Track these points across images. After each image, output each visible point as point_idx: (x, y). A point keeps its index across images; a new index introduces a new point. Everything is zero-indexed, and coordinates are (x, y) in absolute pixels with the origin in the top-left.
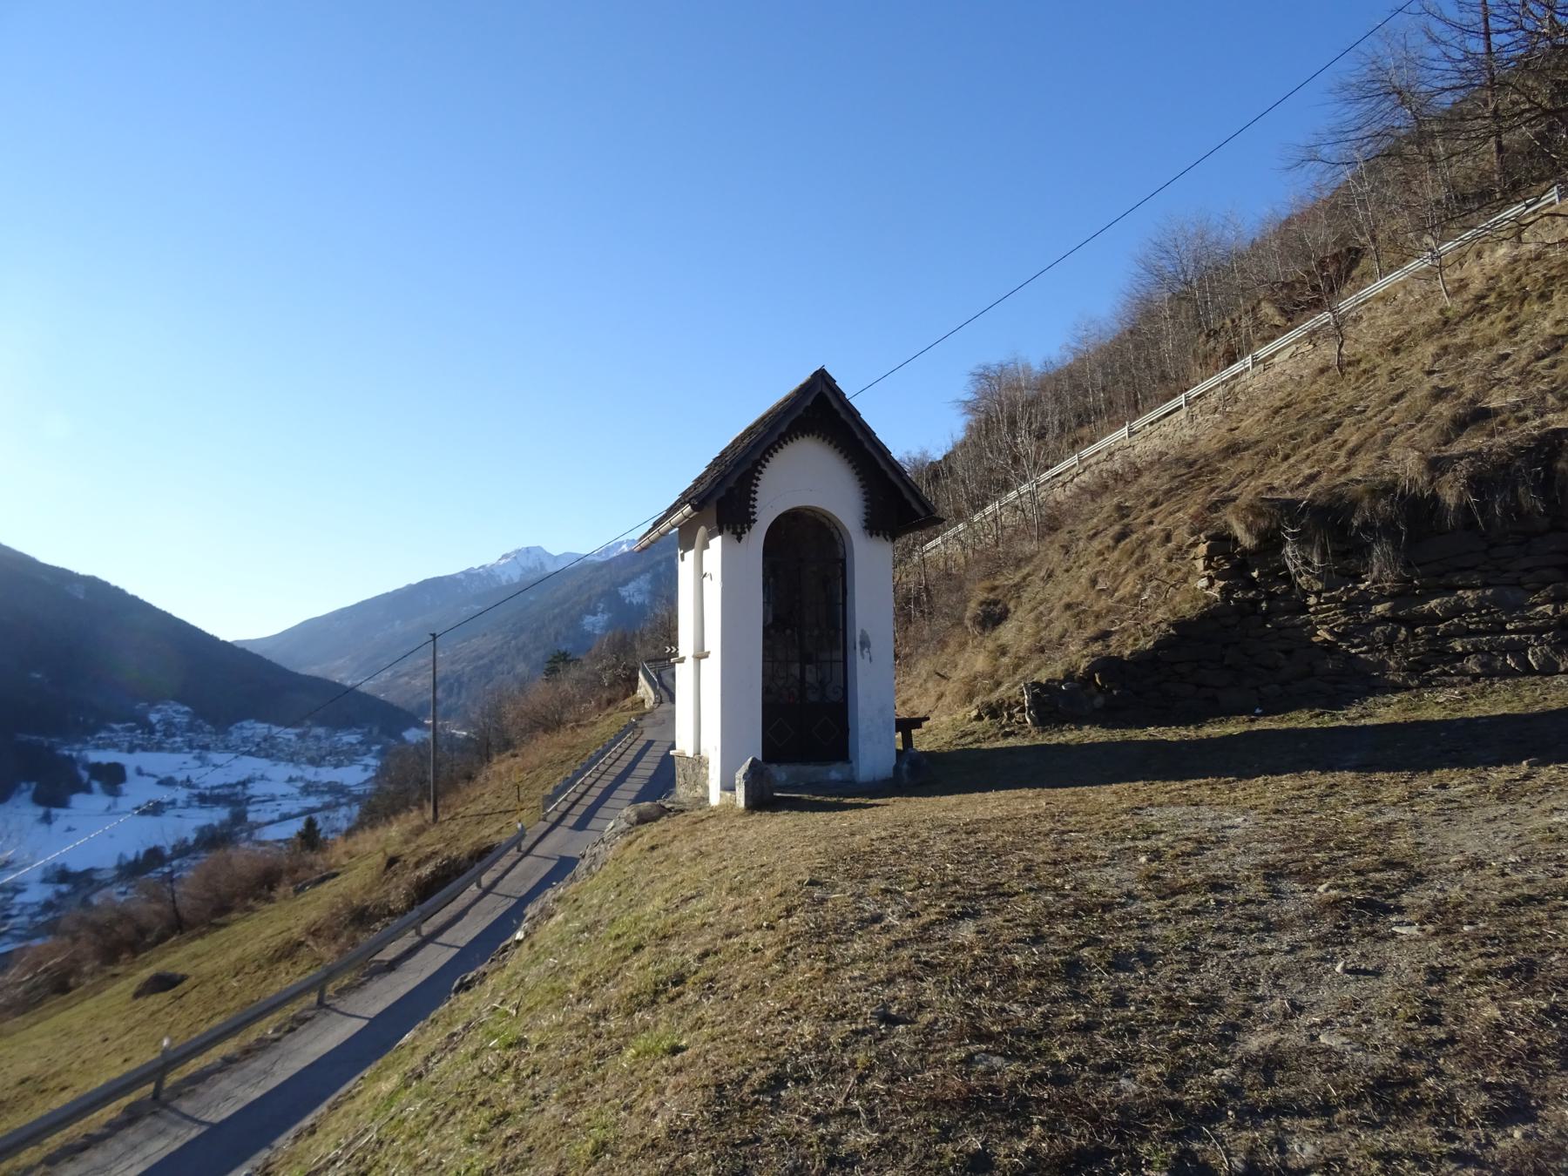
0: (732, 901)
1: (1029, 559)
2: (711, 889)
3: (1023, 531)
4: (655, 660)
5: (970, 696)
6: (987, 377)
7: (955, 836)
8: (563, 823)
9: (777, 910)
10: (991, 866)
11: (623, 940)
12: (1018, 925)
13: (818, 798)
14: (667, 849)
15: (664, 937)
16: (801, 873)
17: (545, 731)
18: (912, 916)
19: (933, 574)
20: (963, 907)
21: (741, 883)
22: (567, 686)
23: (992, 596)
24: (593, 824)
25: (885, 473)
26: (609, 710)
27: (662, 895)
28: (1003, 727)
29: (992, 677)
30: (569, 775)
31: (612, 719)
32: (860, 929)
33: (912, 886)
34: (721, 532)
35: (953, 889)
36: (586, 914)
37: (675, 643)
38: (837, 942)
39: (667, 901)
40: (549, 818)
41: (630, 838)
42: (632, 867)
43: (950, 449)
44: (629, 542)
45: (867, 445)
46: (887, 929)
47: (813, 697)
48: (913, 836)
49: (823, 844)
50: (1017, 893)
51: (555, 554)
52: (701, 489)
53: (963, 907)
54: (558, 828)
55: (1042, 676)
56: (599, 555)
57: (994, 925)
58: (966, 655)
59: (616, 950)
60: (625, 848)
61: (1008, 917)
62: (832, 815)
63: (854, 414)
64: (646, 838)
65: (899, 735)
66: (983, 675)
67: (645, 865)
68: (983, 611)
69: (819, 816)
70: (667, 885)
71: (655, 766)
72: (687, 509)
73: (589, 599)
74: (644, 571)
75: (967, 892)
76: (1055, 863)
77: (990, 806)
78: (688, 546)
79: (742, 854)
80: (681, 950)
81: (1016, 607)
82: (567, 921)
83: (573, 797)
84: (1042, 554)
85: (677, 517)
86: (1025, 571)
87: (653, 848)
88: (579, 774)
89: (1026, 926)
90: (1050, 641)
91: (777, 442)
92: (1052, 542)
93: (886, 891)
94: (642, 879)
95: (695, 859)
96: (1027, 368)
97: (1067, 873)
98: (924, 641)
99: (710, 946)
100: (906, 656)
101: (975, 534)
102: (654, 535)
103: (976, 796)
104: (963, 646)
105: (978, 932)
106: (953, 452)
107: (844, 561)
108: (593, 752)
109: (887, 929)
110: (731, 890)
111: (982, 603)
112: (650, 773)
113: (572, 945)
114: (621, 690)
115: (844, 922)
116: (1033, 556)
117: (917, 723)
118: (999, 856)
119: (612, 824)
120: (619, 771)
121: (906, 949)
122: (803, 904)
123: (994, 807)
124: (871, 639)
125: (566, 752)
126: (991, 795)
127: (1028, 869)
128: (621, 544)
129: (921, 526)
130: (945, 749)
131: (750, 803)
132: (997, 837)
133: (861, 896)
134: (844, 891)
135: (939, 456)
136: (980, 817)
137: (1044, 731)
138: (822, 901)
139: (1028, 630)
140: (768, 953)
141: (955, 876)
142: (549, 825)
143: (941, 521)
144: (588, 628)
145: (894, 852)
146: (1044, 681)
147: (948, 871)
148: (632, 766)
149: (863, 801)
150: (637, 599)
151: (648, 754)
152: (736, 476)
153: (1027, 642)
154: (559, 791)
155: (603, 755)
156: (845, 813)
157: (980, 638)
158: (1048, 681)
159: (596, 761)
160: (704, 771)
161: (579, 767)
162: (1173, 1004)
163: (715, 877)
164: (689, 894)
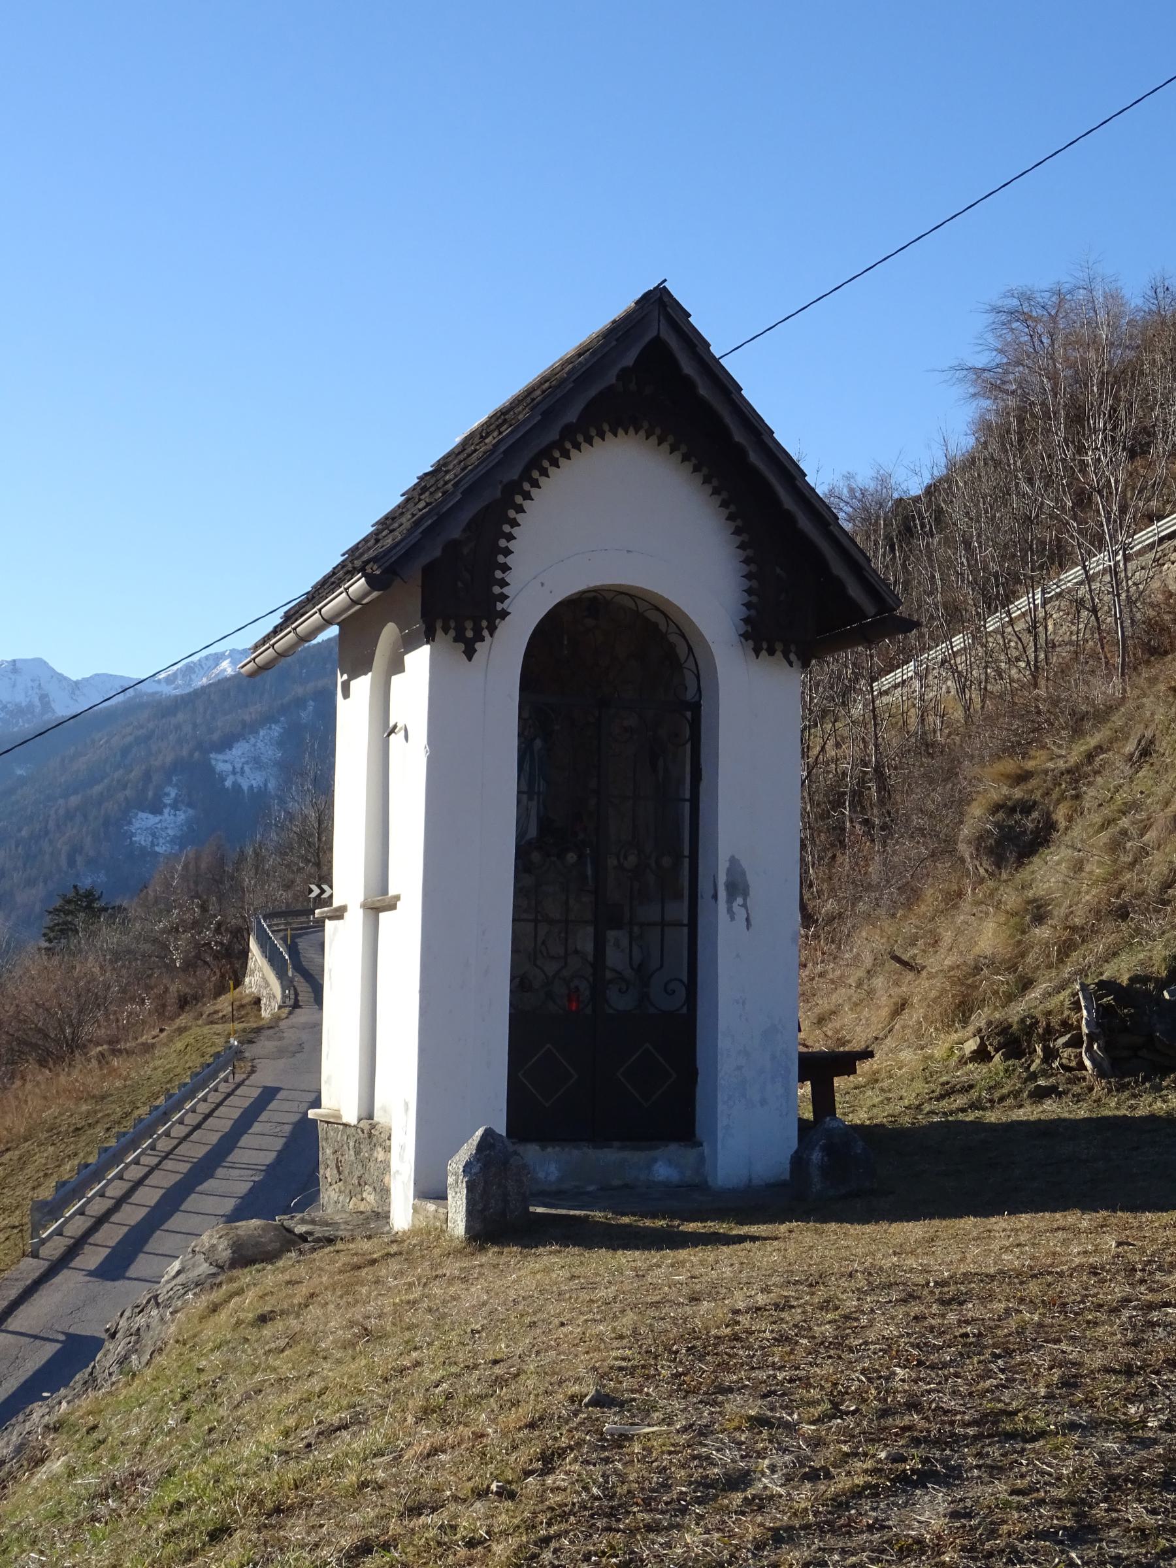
0: (427, 1435)
1: (1102, 715)
2: (383, 1408)
3: (1094, 655)
4: (288, 913)
5: (963, 1010)
6: (1026, 318)
7: (916, 1309)
8: (77, 1262)
9: (523, 1456)
10: (988, 1374)
11: (188, 1516)
12: (1041, 1502)
13: (626, 1220)
14: (293, 1322)
15: (278, 1510)
16: (579, 1380)
17: (42, 1063)
18: (813, 1476)
19: (892, 739)
20: (925, 1461)
21: (449, 1397)
22: (92, 965)
23: (1018, 793)
24: (141, 1266)
25: (789, 518)
26: (182, 1020)
27: (279, 1420)
28: (1033, 1077)
29: (1012, 968)
30: (92, 1160)
31: (188, 1038)
32: (700, 1501)
33: (816, 1412)
34: (429, 637)
35: (906, 1420)
36: (113, 1459)
37: (325, 877)
38: (649, 1528)
39: (286, 1434)
40: (44, 1252)
41: (216, 1296)
42: (216, 1358)
43: (940, 471)
44: (234, 654)
45: (754, 458)
46: (759, 1504)
47: (620, 1001)
48: (825, 1306)
49: (630, 1318)
50: (1042, 1434)
51: (75, 677)
52: (389, 542)
53: (925, 1461)
54: (65, 1274)
55: (1121, 970)
56: (169, 680)
57: (989, 1500)
58: (960, 919)
59: (171, 1535)
60: (202, 1319)
61: (1020, 1483)
62: (655, 1257)
63: (728, 388)
64: (250, 1296)
65: (806, 1089)
66: (993, 964)
67: (244, 1357)
68: (997, 825)
69: (628, 1259)
70: (290, 1398)
71: (279, 1144)
72: (358, 585)
73: (147, 776)
74: (268, 719)
75: (934, 1428)
76: (1129, 1371)
77: (995, 1246)
78: (359, 665)
79: (453, 1336)
80: (312, 1538)
81: (1070, 819)
82: (71, 1473)
83: (98, 1207)
84: (1130, 705)
85: (336, 601)
86: (1092, 741)
87: (263, 1319)
88: (115, 1157)
89: (1059, 1504)
90: (1139, 895)
91: (558, 445)
92: (1153, 681)
93: (759, 1422)
94: (236, 1385)
95: (353, 1345)
96: (1113, 297)
97: (1153, 1393)
98: (869, 887)
99: (374, 1532)
100: (830, 920)
101: (989, 657)
102: (286, 640)
103: (968, 1223)
104: (953, 898)
105: (955, 1515)
106: (947, 479)
107: (696, 707)
108: (143, 1111)
109: (759, 1504)
110: (426, 1412)
111: (996, 808)
112: (269, 1158)
113: (79, 1525)
114: (209, 977)
115: (665, 1487)
116: (1110, 709)
117: (846, 1062)
118: (1009, 1353)
119: (176, 1265)
120: (200, 1152)
121: (798, 1546)
122: (579, 1444)
123: (1006, 1249)
124: (751, 878)
125: (85, 1108)
126: (999, 1223)
127: (1069, 1383)
128: (218, 658)
129: (869, 636)
130: (906, 1121)
131: (478, 1226)
132: (1007, 1311)
133: (704, 1432)
134: (668, 1420)
135: (915, 488)
136: (972, 1268)
137: (1121, 1088)
138: (621, 1440)
139: (1095, 868)
140: (498, 1548)
141: (911, 1395)
142: (43, 1265)
143: (909, 625)
144: (141, 839)
145: (782, 1339)
146: (1124, 980)
147: (896, 1383)
148: (229, 1142)
149: (722, 1228)
150: (252, 780)
151: (264, 1116)
152: (466, 516)
153: (1090, 896)
154: (69, 1192)
155: (165, 1116)
156: (683, 1254)
157: (990, 883)
158: (1132, 980)
159: (149, 1130)
160: (380, 1154)
161: (113, 1143)
162: (184, 1069)
163: (393, 1384)
164: (335, 1420)
